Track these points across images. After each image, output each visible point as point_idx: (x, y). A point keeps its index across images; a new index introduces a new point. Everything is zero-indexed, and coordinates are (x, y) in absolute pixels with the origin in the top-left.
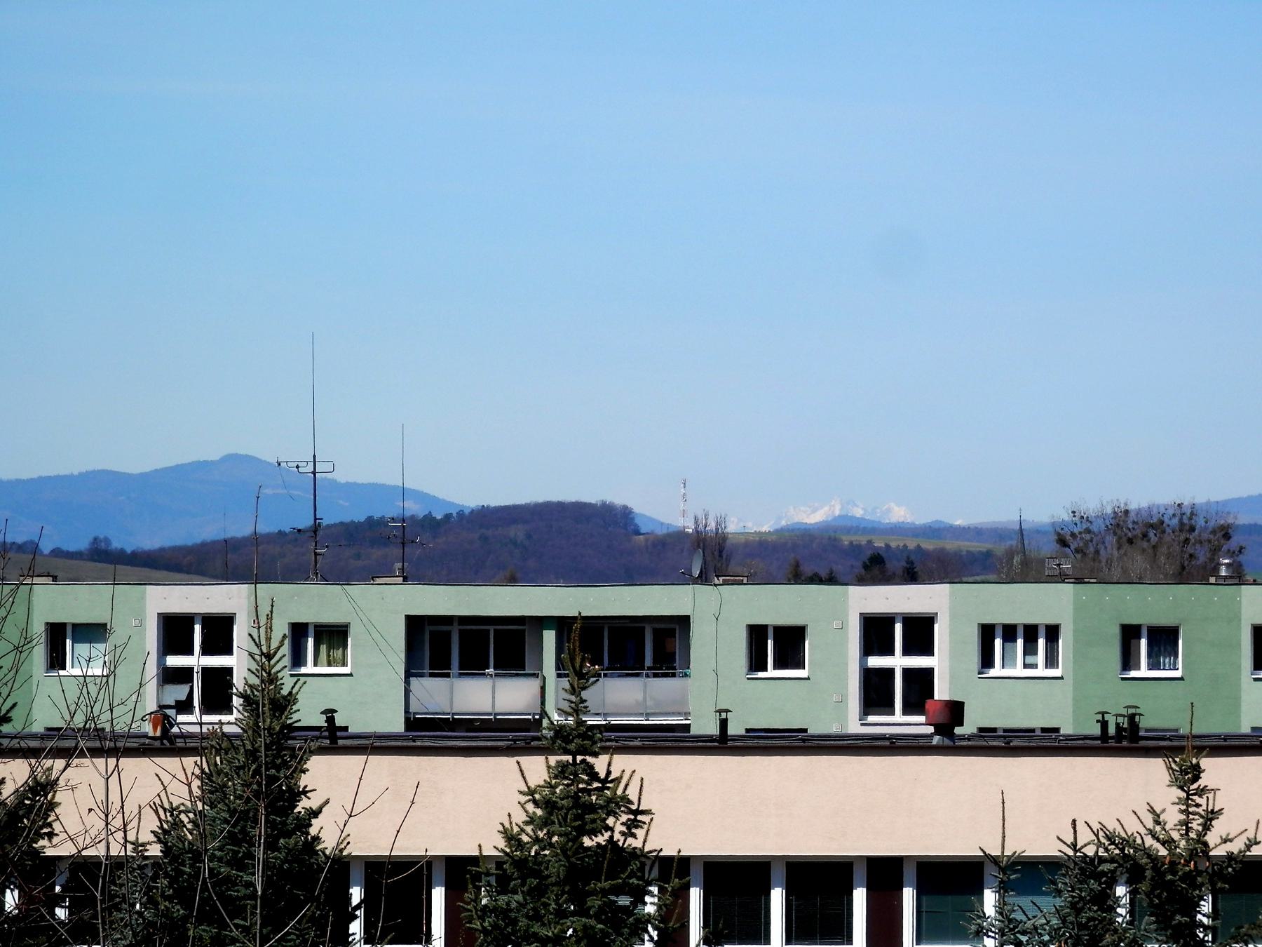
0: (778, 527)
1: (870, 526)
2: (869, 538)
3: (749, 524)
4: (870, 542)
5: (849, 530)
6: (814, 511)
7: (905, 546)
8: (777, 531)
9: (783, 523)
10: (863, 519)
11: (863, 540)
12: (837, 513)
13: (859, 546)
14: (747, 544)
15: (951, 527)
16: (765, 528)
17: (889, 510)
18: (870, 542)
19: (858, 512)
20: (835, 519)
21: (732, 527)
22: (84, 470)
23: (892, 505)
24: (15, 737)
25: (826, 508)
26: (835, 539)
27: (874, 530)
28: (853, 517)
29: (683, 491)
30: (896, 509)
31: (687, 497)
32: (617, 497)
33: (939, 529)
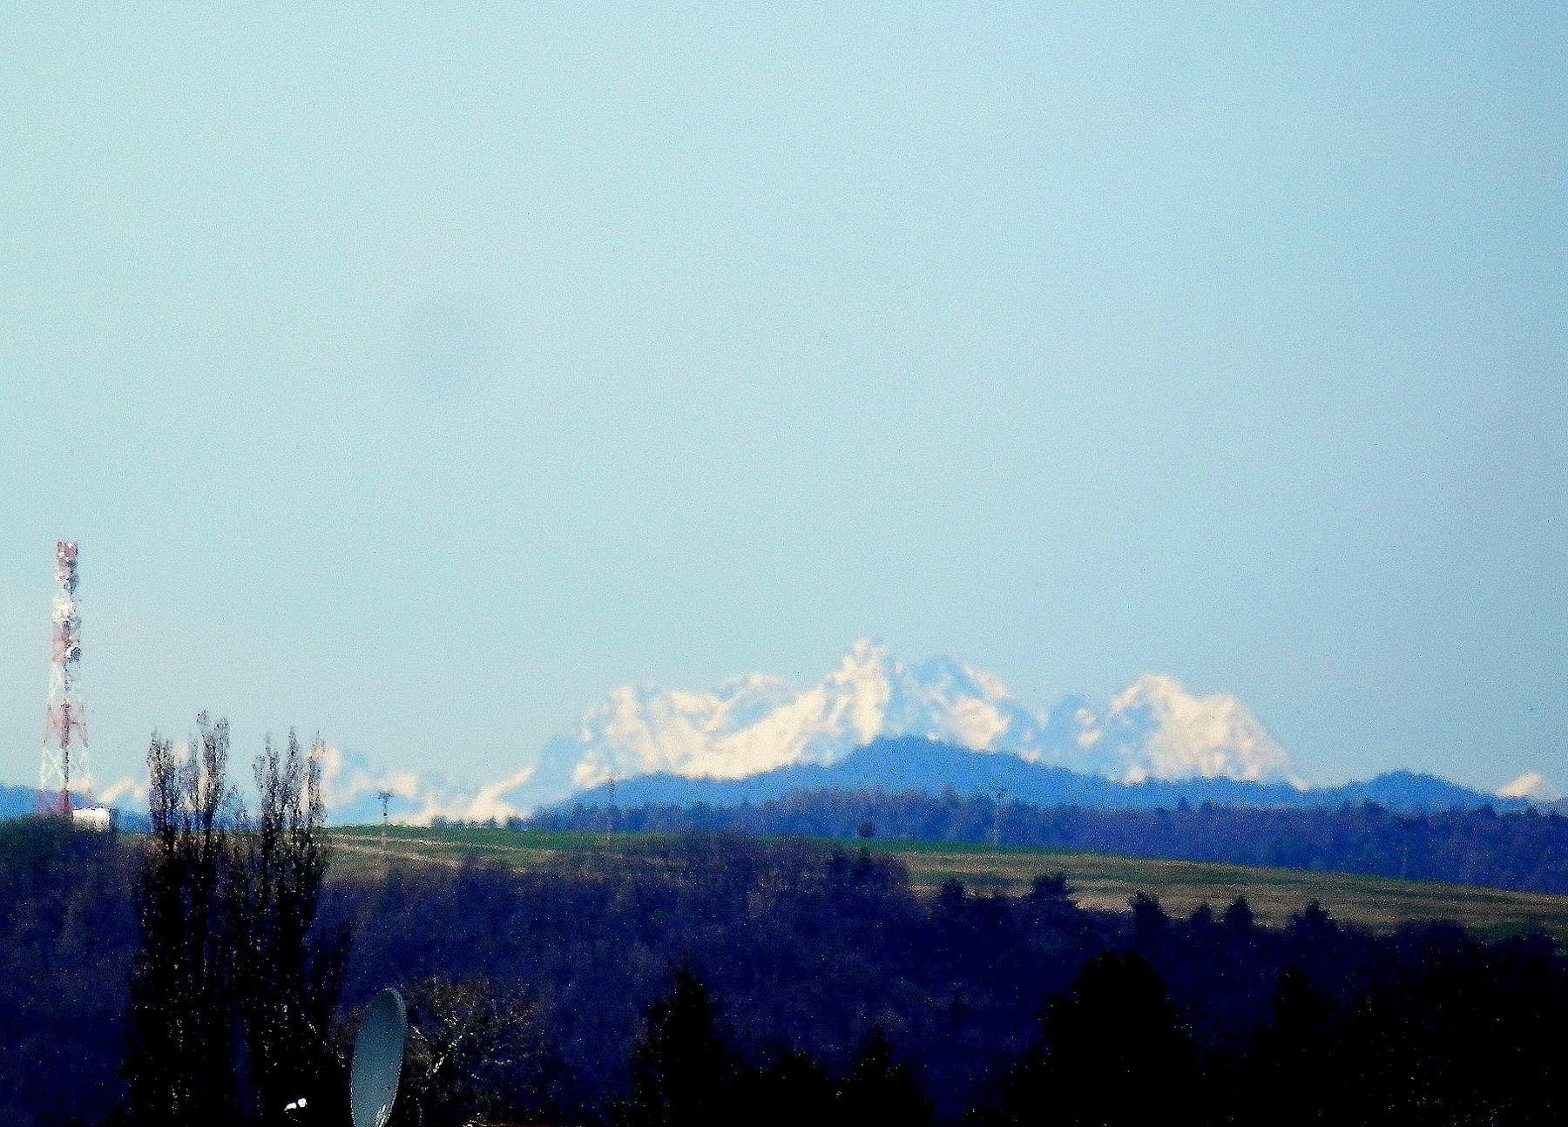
0: (556, 797)
1: (1045, 801)
2: (1051, 862)
3: (404, 784)
4: (1051, 887)
5: (934, 820)
6: (751, 712)
7: (1240, 911)
8: (549, 825)
9: (586, 776)
10: (1006, 761)
11: (1017, 873)
12: (869, 726)
13: (995, 910)
14: (397, 892)
15: (1487, 810)
16: (487, 807)
17: (1144, 717)
18: (1051, 887)
19: (980, 727)
20: (861, 757)
21: (340, 800)
22: (1416, 770)
23: (1165, 687)
24: (636, 852)
25: (810, 702)
26: (866, 869)
27: (1067, 821)
28: (954, 756)
29: (63, 607)
30: (1183, 707)
31: (86, 638)
32: (1389, 767)
33: (1416, 827)
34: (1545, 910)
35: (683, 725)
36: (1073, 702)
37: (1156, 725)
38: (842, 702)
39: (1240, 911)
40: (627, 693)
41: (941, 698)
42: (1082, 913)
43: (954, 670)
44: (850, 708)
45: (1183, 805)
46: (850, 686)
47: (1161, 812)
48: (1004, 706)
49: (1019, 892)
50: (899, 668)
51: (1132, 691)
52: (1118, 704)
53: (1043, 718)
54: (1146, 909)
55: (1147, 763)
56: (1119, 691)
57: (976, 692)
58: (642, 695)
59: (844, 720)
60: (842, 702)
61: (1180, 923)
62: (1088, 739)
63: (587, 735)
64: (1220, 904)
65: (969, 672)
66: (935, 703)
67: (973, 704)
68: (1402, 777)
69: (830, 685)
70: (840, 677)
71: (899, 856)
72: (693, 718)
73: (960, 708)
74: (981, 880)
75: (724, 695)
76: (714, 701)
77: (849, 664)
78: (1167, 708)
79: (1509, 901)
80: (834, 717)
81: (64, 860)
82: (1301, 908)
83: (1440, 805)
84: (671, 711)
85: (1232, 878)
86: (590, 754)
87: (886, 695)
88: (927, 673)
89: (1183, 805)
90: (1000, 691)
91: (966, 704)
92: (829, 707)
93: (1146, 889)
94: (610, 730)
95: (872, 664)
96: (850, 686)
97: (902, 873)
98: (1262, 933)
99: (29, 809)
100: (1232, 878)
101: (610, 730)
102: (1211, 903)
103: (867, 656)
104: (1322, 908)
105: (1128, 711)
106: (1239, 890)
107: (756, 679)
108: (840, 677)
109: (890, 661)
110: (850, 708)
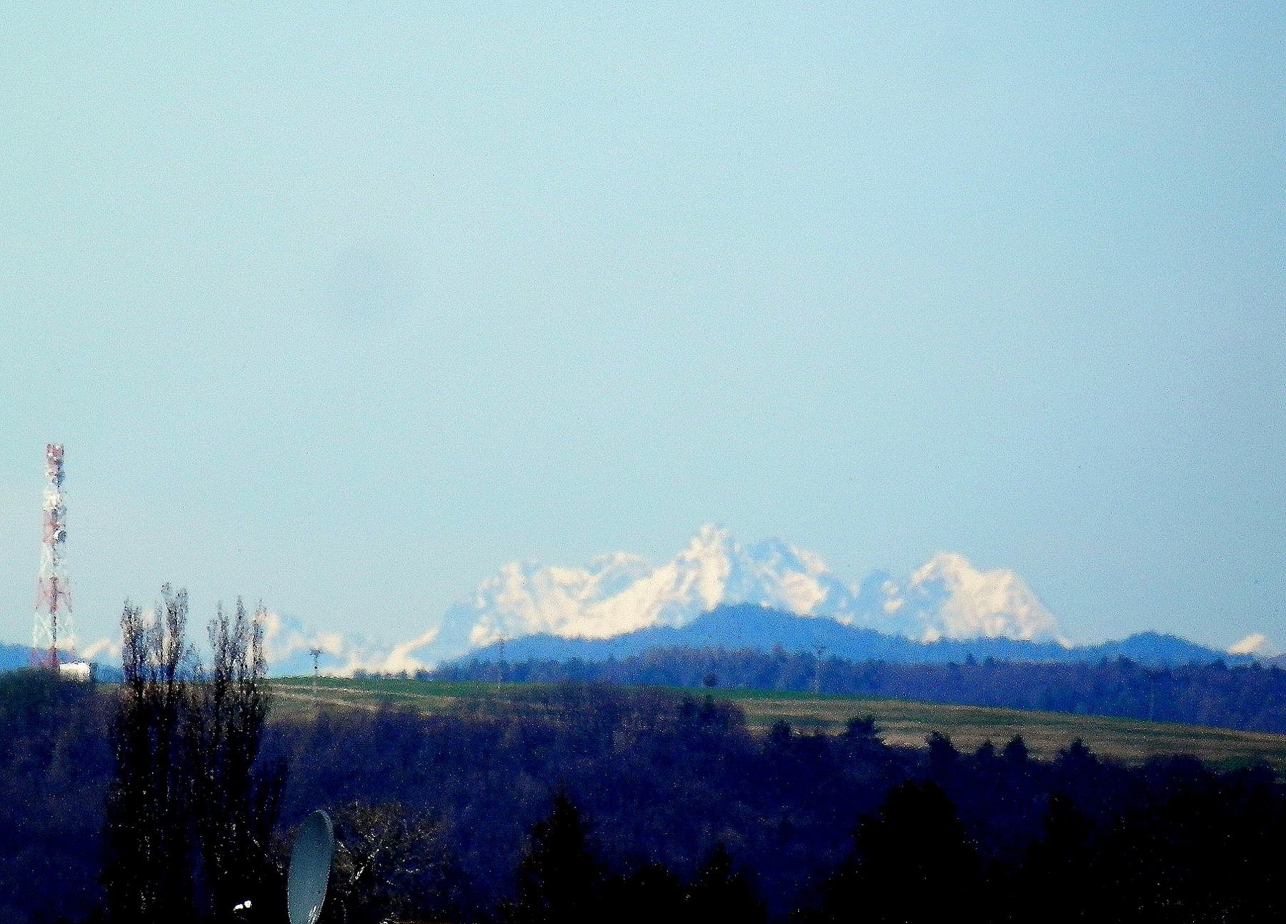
0: (456, 653)
1: (857, 657)
2: (862, 707)
3: (331, 643)
4: (862, 728)
5: (766, 672)
6: (616, 584)
7: (1017, 747)
8: (450, 676)
9: (481, 636)
10: (825, 624)
11: (834, 716)
12: (713, 595)
13: (816, 746)
14: (325, 731)
15: (1219, 664)
16: (399, 661)
17: (938, 588)
18: (862, 728)
19: (803, 596)
20: (706, 621)
21: (279, 656)
22: (1162, 631)
23: (956, 564)
24: (521, 699)
25: (664, 576)
26: (710, 713)
27: (875, 673)
28: (782, 620)
29: (51, 498)
30: (970, 580)
31: (71, 523)
32: (1139, 628)
33: (1161, 678)
34: (1267, 746)
35: (560, 594)
36: (880, 576)
37: (948, 594)
38: (691, 576)
39: (1017, 747)
40: (514, 569)
41: (772, 573)
42: (887, 749)
43: (783, 549)
44: (697, 580)
45: (971, 660)
46: (697, 563)
47: (953, 666)
48: (823, 579)
49: (836, 732)
50: (737, 547)
51: (929, 567)
52: (917, 577)
53: (855, 589)
54: (940, 745)
55: (941, 626)
56: (918, 567)
57: (800, 567)
58: (527, 570)
59: (692, 591)
60: (691, 576)
61: (968, 756)
62: (892, 606)
63: (482, 603)
64: (1001, 742)
65: (795, 551)
66: (766, 576)
67: (798, 577)
68: (1150, 637)
69: (681, 562)
70: (689, 555)
71: (737, 702)
72: (568, 589)
73: (787, 581)
74: (804, 722)
75: (594, 570)
76: (586, 575)
77: (697, 544)
78: (957, 580)
79: (1237, 739)
80: (684, 587)
81: (52, 705)
82: (1067, 744)
83: (1181, 660)
84: (551, 583)
85: (1010, 720)
86: (484, 619)
87: (727, 570)
88: (760, 552)
89: (971, 660)
90: (820, 566)
91: (792, 577)
92: (680, 580)
93: (940, 729)
94: (501, 598)
95: (715, 545)
96: (697, 563)
97: (740, 716)
98: (1035, 765)
99: (24, 663)
100: (1010, 720)
101: (501, 598)
102: (994, 740)
103: (711, 538)
104: (1084, 744)
105: (925, 583)
106: (1017, 729)
107: (620, 557)
108: (689, 555)
109: (730, 542)
110: (697, 580)
